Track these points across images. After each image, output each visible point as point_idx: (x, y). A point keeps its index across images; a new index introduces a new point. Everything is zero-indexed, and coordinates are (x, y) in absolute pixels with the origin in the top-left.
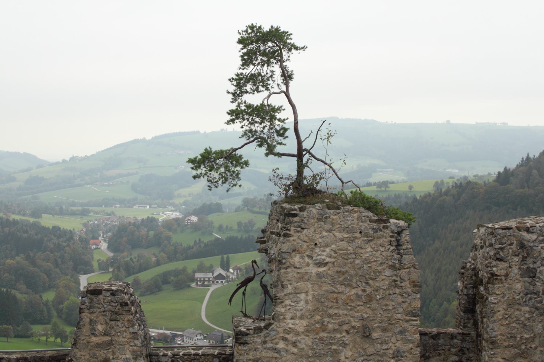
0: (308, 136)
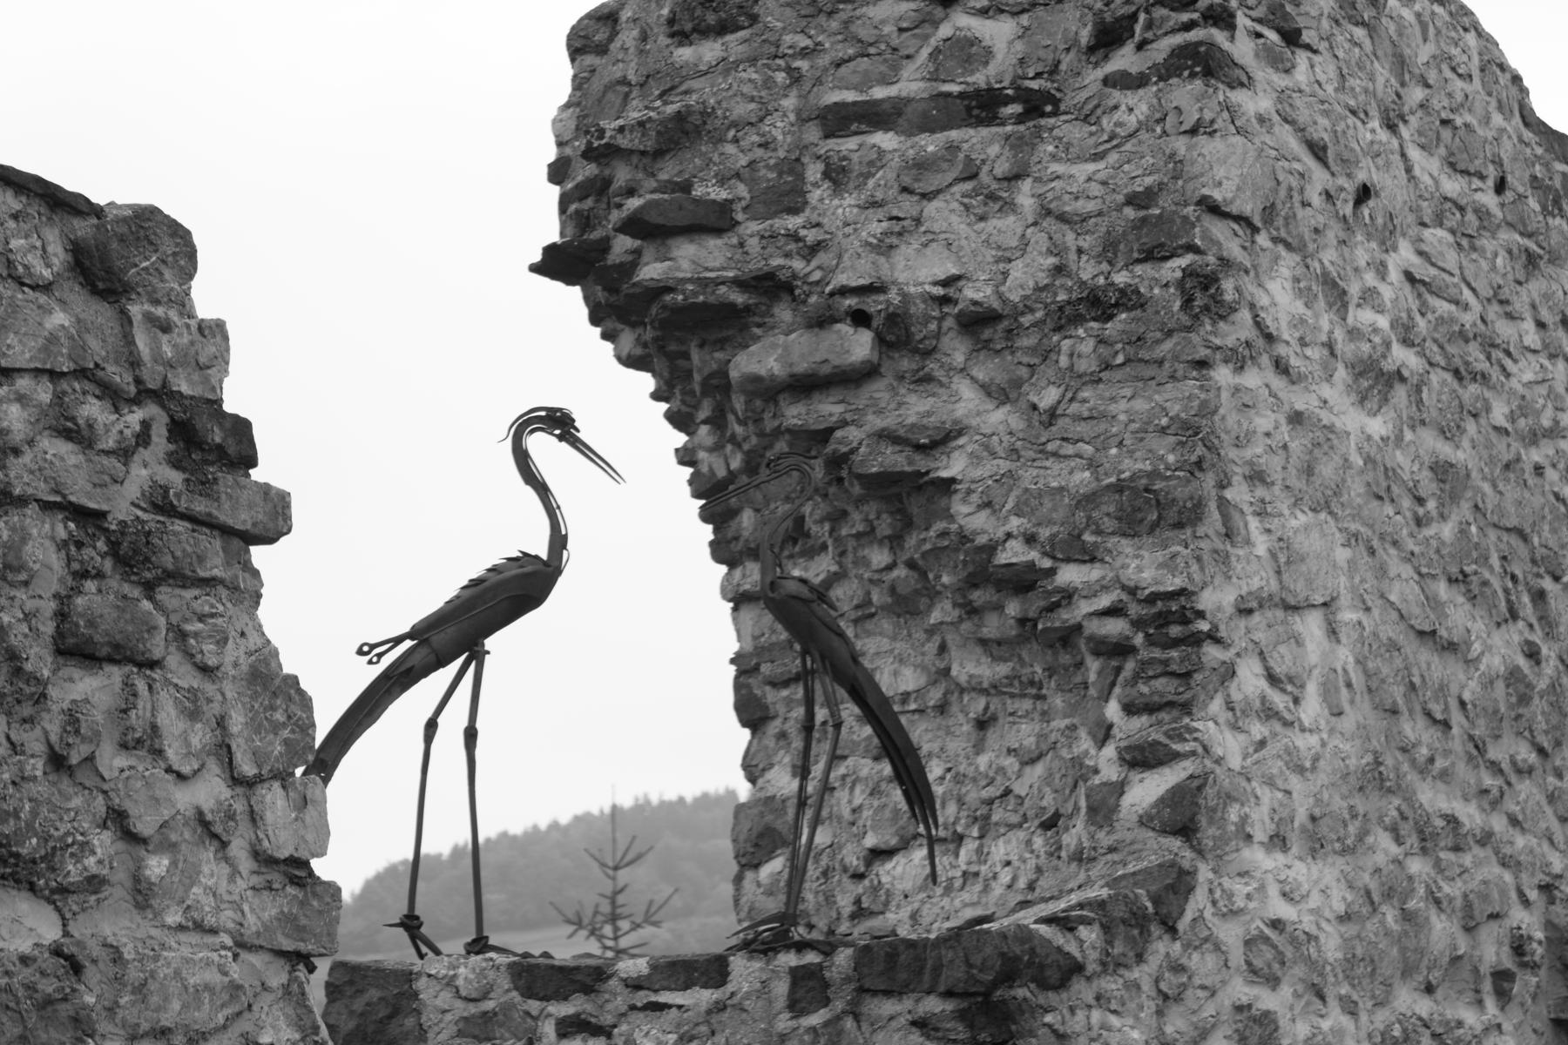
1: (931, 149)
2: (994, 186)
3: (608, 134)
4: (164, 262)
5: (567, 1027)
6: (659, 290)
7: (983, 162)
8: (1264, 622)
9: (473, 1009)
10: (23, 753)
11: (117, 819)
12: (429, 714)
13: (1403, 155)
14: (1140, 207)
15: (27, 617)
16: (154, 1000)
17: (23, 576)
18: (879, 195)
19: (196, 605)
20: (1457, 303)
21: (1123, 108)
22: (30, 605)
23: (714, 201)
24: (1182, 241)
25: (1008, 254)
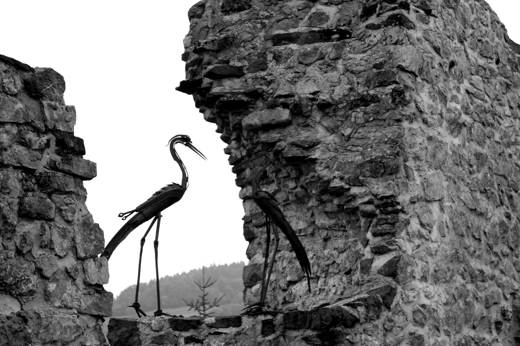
1: (309, 49)
2: (330, 61)
3: (202, 44)
4: (54, 87)
5: (188, 340)
6: (218, 96)
7: (326, 54)
8: (419, 206)
9: (157, 334)
11: (39, 271)
12: (142, 236)
13: (465, 51)
14: (378, 69)
15: (9, 204)
16: (51, 331)
17: (8, 191)
18: (292, 65)
19: (65, 200)
20: (483, 100)
21: (372, 36)
22: (10, 200)
25: (334, 84)
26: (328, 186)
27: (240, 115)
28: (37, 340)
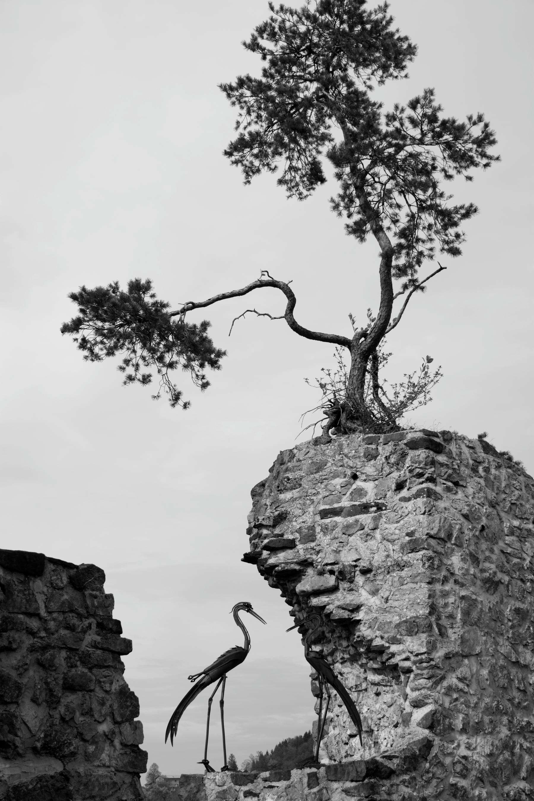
0: (273, 316)
1: (351, 521)
2: (369, 531)
3: (260, 521)
4: (96, 579)
5: (248, 794)
6: (274, 566)
7: (366, 525)
8: (455, 661)
9: (220, 789)
10: (53, 718)
11: (80, 735)
12: (210, 696)
13: (498, 515)
14: (409, 536)
15: (55, 679)
16: (90, 788)
17: (54, 668)
18: (336, 536)
19: (104, 673)
20: (520, 558)
21: (404, 507)
22: (56, 676)
23: (289, 539)
24: (422, 547)
25: (373, 552)
26: (371, 644)
27: (294, 582)
28: (78, 796)
